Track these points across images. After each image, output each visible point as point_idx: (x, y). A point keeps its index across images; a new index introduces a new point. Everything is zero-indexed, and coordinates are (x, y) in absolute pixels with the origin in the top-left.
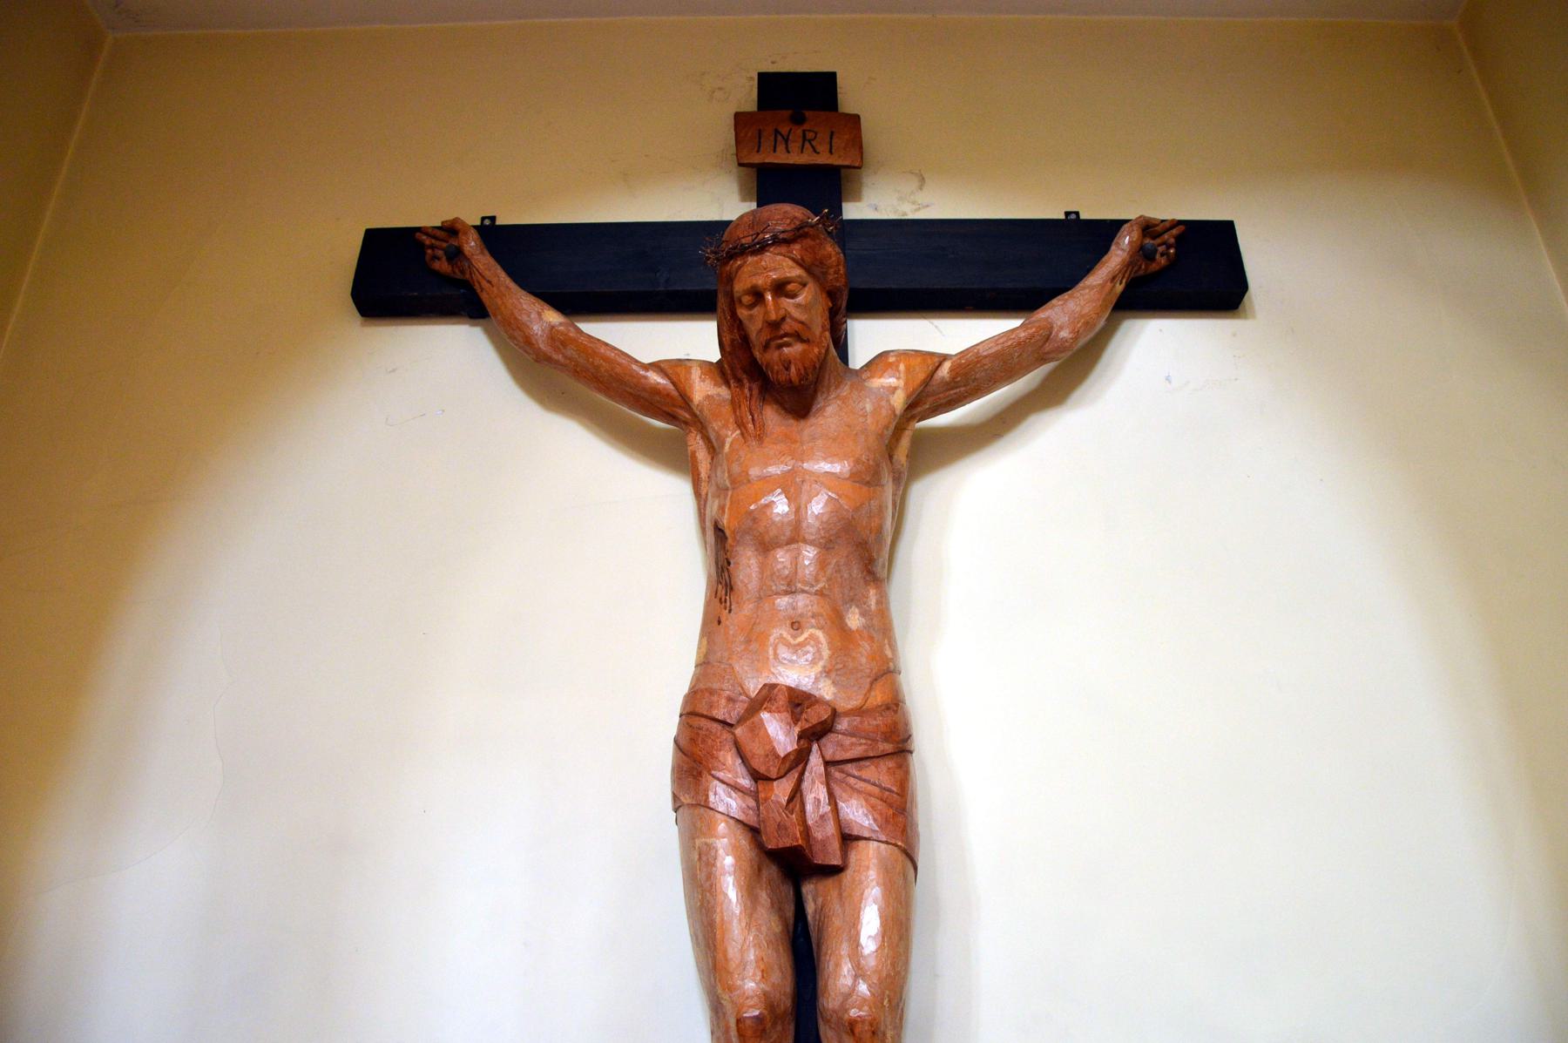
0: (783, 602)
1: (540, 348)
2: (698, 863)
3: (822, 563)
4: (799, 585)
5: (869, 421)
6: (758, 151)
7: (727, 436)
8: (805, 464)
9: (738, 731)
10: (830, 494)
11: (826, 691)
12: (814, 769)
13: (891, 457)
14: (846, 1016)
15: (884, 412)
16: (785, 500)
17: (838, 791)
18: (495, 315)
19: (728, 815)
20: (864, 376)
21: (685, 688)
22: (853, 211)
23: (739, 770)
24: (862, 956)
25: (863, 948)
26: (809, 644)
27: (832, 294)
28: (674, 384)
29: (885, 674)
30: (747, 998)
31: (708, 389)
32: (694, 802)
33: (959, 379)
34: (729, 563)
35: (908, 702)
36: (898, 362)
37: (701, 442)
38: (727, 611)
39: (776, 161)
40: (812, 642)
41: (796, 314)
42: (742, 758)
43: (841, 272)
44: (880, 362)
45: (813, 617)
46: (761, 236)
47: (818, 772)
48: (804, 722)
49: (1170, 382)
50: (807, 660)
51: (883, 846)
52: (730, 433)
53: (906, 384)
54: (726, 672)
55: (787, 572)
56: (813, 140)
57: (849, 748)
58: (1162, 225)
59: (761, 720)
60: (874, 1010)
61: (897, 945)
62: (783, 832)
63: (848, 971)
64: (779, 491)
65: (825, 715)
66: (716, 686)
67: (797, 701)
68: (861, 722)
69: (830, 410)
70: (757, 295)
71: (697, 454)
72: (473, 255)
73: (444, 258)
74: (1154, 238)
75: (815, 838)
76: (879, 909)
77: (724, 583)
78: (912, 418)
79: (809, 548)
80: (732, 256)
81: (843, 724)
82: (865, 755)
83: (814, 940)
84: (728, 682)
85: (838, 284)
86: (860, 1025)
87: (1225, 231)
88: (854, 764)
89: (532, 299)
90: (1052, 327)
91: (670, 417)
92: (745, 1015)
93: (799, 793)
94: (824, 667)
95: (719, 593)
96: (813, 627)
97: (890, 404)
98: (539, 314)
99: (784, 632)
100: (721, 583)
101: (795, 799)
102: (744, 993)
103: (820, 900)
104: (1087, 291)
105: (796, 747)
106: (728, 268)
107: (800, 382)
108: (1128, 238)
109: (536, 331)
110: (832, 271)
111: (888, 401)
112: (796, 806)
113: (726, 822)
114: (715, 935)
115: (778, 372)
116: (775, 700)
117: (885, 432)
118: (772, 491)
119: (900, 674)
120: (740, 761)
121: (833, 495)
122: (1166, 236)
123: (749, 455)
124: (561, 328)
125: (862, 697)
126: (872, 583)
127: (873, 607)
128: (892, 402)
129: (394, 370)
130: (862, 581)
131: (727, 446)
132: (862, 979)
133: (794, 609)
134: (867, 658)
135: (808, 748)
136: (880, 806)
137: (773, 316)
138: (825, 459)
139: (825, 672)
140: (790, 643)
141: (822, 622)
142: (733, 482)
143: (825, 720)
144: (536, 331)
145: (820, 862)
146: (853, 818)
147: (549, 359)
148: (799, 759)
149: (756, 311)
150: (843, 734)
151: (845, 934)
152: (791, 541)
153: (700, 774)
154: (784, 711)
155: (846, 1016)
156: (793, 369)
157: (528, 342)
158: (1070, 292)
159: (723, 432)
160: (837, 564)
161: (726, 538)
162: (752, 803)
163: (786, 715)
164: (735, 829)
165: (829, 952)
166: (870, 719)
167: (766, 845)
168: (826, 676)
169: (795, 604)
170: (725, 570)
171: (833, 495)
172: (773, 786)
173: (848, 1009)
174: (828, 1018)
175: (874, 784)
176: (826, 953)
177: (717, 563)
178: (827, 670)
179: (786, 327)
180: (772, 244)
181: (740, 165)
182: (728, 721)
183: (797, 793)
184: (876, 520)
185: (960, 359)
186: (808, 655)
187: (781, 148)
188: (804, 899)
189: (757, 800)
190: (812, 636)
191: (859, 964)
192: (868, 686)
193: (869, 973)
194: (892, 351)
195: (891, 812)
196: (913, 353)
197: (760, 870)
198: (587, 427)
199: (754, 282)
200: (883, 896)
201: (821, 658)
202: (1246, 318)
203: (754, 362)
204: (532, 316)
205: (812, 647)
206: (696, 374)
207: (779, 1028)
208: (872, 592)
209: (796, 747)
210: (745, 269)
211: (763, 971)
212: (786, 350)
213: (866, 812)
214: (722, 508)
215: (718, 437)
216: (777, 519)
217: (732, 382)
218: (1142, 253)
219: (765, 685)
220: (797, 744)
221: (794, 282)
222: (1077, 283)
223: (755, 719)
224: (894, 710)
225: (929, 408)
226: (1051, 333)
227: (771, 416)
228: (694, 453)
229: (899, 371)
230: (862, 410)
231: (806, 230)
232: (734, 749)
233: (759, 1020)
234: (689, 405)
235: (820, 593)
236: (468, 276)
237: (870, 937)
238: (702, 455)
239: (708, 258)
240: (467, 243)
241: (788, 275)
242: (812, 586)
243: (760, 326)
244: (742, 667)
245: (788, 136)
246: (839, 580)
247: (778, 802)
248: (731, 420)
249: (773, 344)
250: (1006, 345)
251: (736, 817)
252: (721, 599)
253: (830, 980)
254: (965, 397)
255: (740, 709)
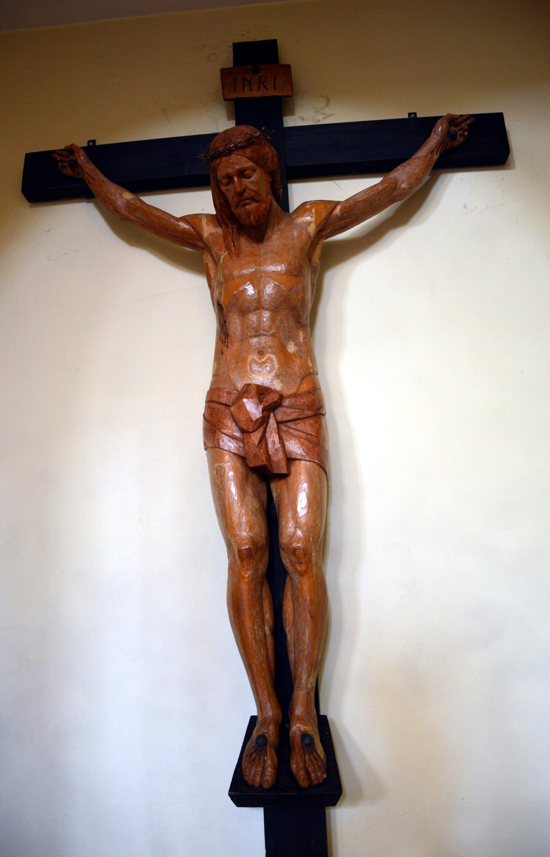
0: (254, 341)
1: (122, 213)
2: (216, 476)
3: (273, 320)
4: (262, 332)
5: (295, 242)
6: (234, 91)
7: (221, 255)
8: (261, 268)
9: (232, 409)
10: (275, 283)
11: (277, 386)
12: (272, 426)
13: (310, 260)
14: (291, 547)
15: (304, 236)
16: (252, 287)
17: (284, 436)
18: (98, 197)
19: (230, 451)
20: (294, 217)
21: (207, 388)
22: (290, 122)
23: (234, 428)
24: (298, 517)
25: (299, 513)
26: (267, 362)
27: (271, 174)
28: (193, 228)
29: (308, 375)
30: (243, 540)
31: (211, 229)
32: (213, 446)
33: (345, 215)
34: (225, 322)
35: (322, 388)
36: (311, 208)
37: (210, 258)
38: (226, 347)
39: (244, 96)
40: (269, 361)
41: (251, 187)
42: (235, 423)
43: (275, 161)
44: (303, 208)
45: (269, 348)
46: (228, 146)
47: (273, 427)
48: (265, 402)
49: (466, 208)
50: (267, 371)
51: (308, 463)
52: (223, 253)
53: (316, 219)
54: (226, 379)
55: (255, 325)
56: (265, 82)
57: (289, 414)
58: (460, 118)
59: (243, 403)
60: (305, 543)
61: (316, 511)
62: (257, 458)
63: (292, 525)
64: (249, 282)
65: (276, 398)
66: (222, 386)
67: (261, 392)
68: (295, 401)
69: (275, 237)
70: (230, 178)
71: (209, 265)
72: (83, 164)
73: (68, 167)
74: (456, 126)
75: (273, 461)
76: (306, 494)
77: (224, 332)
78: (322, 237)
79: (265, 312)
80: (214, 158)
81: (286, 402)
82: (298, 417)
83: (277, 510)
84: (228, 384)
85: (274, 168)
86: (298, 551)
87: (498, 118)
88: (293, 422)
89: (116, 186)
90: (397, 182)
91: (194, 246)
92: (242, 548)
93: (264, 438)
94: (276, 373)
95: (222, 338)
96: (269, 353)
97: (307, 232)
98: (121, 195)
99: (255, 357)
100: (222, 332)
101: (263, 442)
102: (241, 538)
103: (279, 491)
104: (417, 160)
105: (261, 415)
106: (213, 165)
107: (256, 224)
108: (440, 128)
109: (120, 204)
110: (270, 161)
111: (307, 230)
112: (263, 445)
113: (229, 455)
114: (226, 510)
115: (244, 219)
116: (250, 392)
117: (305, 247)
118: (245, 283)
119: (317, 374)
120: (235, 424)
121: (277, 283)
122: (463, 125)
123: (232, 265)
124: (133, 201)
125: (296, 388)
126: (301, 328)
127: (301, 341)
128: (308, 230)
129: (49, 231)
130: (295, 329)
131: (222, 260)
132: (299, 529)
133: (260, 344)
134: (298, 368)
135: (267, 415)
136: (306, 442)
137: (239, 189)
138: (272, 264)
139: (276, 376)
140: (258, 362)
141: (274, 350)
142: (225, 280)
143: (276, 401)
144: (120, 204)
145: (276, 472)
146: (292, 450)
147: (128, 219)
148: (264, 421)
149: (229, 187)
150: (287, 407)
151: (290, 507)
152: (256, 309)
153: (215, 432)
154: (255, 398)
155: (291, 547)
156: (252, 217)
157: (116, 210)
158: (407, 161)
159: (219, 253)
160: (281, 320)
161: (223, 309)
162: (241, 445)
163: (256, 400)
164: (234, 458)
165: (283, 516)
166: (300, 399)
167: (249, 465)
168: (277, 378)
169: (260, 342)
170: (224, 326)
171: (277, 283)
172: (251, 436)
173: (292, 543)
174: (284, 548)
175: (303, 432)
176: (281, 517)
177: (220, 323)
178: (277, 375)
179: (246, 195)
180: (235, 150)
181: (225, 100)
182: (228, 404)
183: (263, 439)
184: (301, 295)
185: (346, 203)
186: (268, 368)
187: (247, 88)
188: (272, 491)
189: (244, 443)
190: (269, 358)
191: (297, 521)
192: (299, 382)
193: (302, 525)
194: (308, 202)
195: (311, 446)
196: (319, 202)
197: (247, 477)
198: (154, 254)
199: (227, 171)
200: (308, 487)
201: (274, 369)
202: (510, 169)
203: (232, 213)
204: (117, 196)
205: (270, 363)
206: (204, 221)
207: (260, 553)
208: (301, 333)
209: (261, 415)
210: (222, 164)
211: (250, 527)
212: (247, 207)
213: (298, 446)
214: (220, 294)
215: (217, 255)
216: (248, 298)
217: (223, 225)
218: (449, 136)
219: (245, 385)
220: (262, 414)
221: (248, 170)
222: (412, 156)
223: (240, 402)
224: (313, 394)
225: (330, 232)
226: (397, 185)
227: (244, 243)
228: (207, 264)
229: (312, 213)
230: (292, 236)
231: (253, 140)
232: (231, 418)
233: (249, 550)
234: (202, 239)
235: (273, 335)
236: (82, 176)
237: (302, 508)
238: (211, 265)
239: (203, 160)
240: (80, 158)
241: (245, 166)
242: (268, 332)
243: (233, 195)
244: (234, 376)
245: (251, 81)
246: (283, 328)
247: (254, 444)
248: (223, 246)
249: (241, 204)
250: (371, 194)
251: (234, 452)
252: (223, 341)
253: (283, 530)
254: (350, 224)
255: (233, 397)
